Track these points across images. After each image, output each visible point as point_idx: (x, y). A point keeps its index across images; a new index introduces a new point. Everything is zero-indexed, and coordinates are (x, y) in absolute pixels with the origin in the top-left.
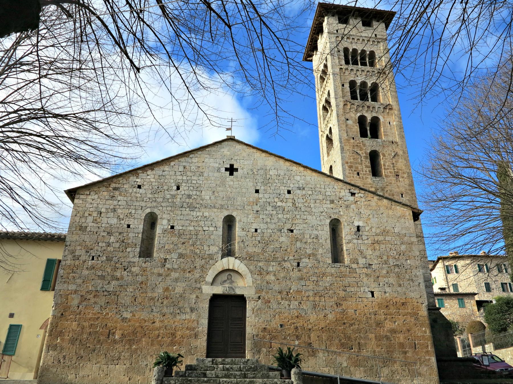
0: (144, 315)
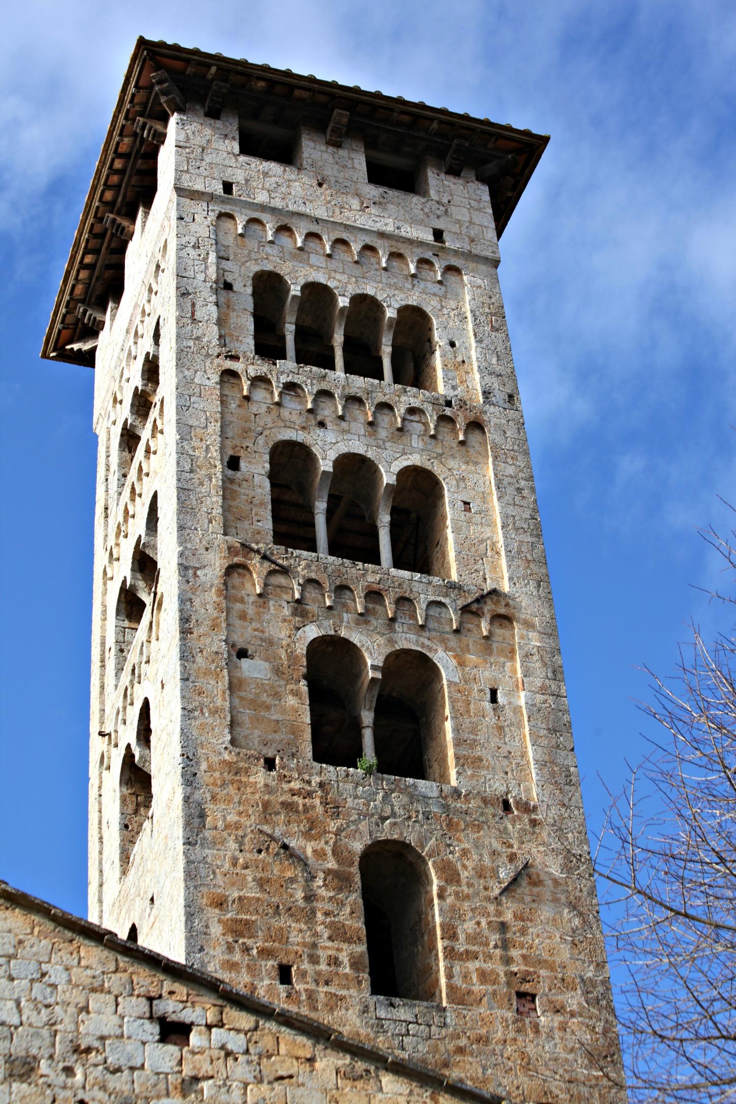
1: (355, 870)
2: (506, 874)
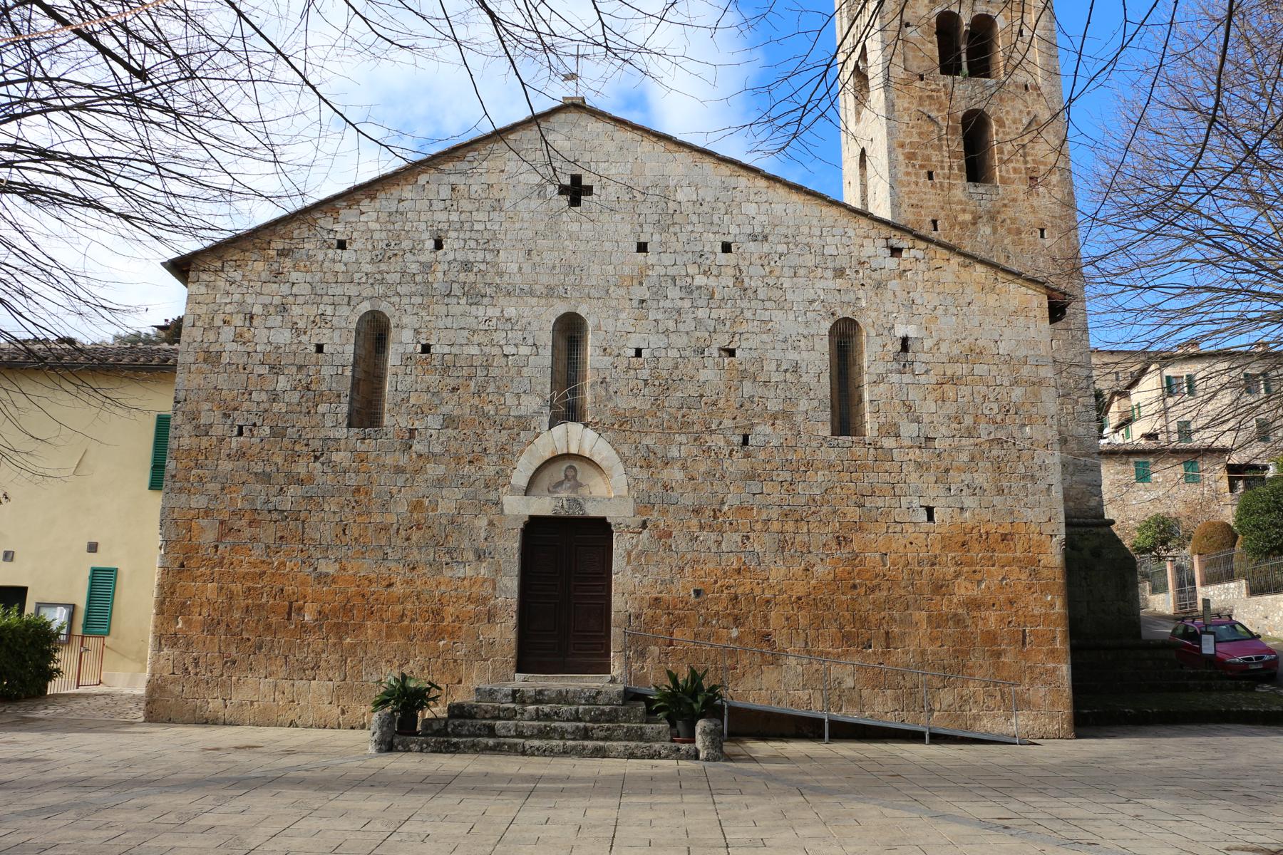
2: (1025, 121)
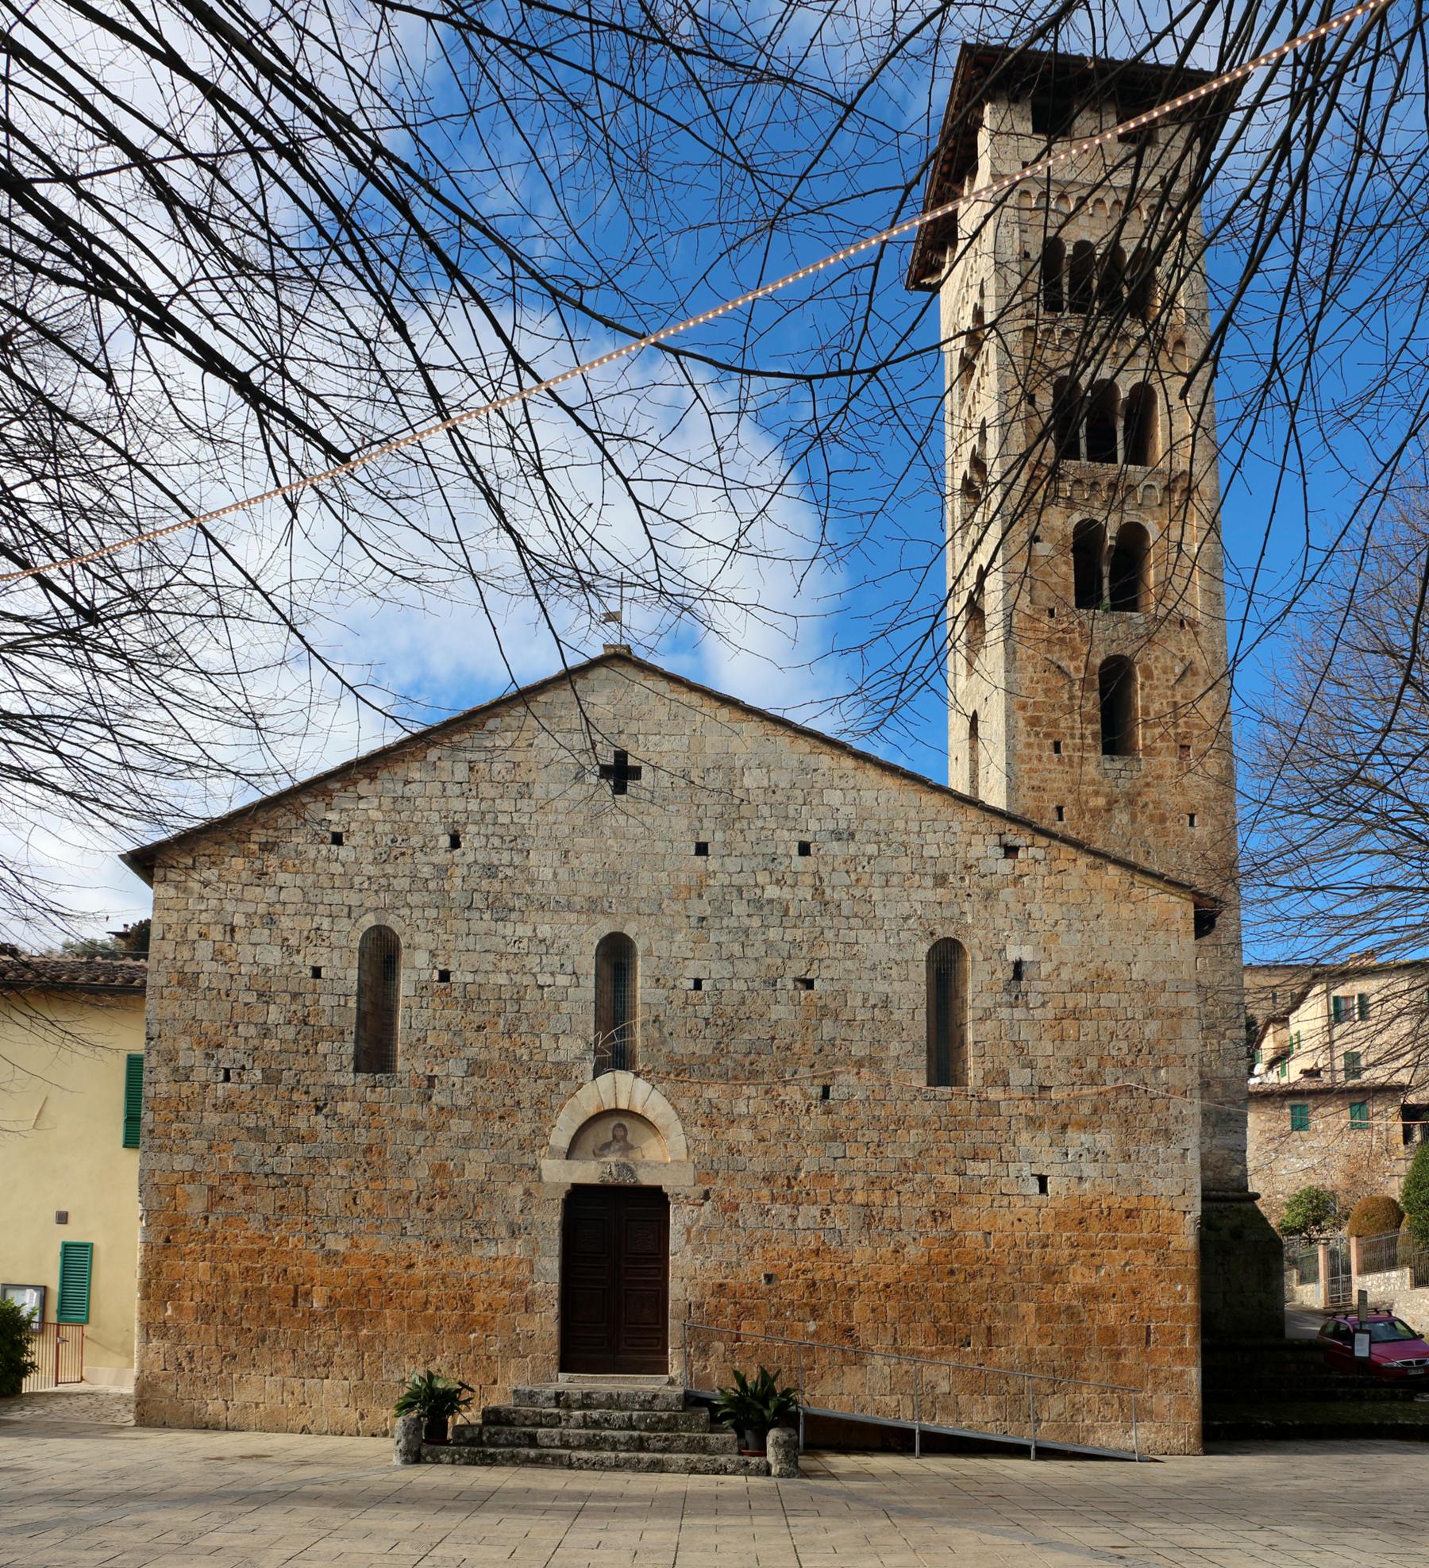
0: (381, 1244)
1: (1096, 677)
2: (1178, 670)
